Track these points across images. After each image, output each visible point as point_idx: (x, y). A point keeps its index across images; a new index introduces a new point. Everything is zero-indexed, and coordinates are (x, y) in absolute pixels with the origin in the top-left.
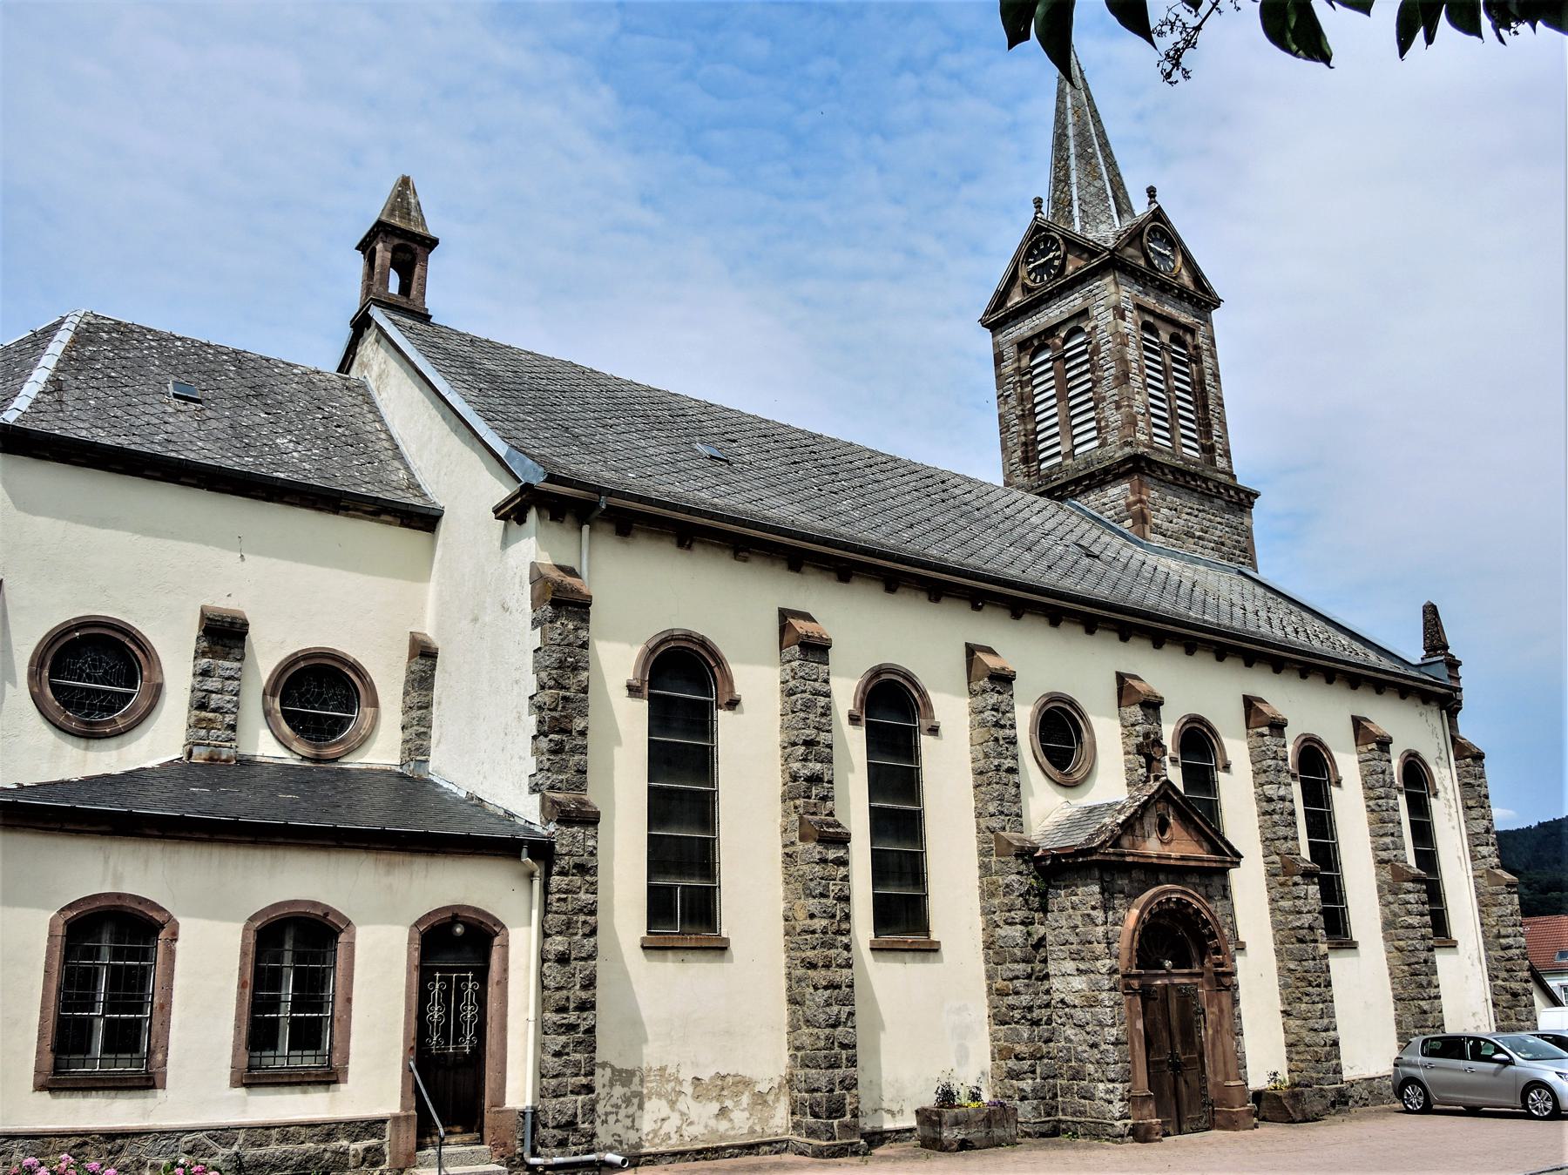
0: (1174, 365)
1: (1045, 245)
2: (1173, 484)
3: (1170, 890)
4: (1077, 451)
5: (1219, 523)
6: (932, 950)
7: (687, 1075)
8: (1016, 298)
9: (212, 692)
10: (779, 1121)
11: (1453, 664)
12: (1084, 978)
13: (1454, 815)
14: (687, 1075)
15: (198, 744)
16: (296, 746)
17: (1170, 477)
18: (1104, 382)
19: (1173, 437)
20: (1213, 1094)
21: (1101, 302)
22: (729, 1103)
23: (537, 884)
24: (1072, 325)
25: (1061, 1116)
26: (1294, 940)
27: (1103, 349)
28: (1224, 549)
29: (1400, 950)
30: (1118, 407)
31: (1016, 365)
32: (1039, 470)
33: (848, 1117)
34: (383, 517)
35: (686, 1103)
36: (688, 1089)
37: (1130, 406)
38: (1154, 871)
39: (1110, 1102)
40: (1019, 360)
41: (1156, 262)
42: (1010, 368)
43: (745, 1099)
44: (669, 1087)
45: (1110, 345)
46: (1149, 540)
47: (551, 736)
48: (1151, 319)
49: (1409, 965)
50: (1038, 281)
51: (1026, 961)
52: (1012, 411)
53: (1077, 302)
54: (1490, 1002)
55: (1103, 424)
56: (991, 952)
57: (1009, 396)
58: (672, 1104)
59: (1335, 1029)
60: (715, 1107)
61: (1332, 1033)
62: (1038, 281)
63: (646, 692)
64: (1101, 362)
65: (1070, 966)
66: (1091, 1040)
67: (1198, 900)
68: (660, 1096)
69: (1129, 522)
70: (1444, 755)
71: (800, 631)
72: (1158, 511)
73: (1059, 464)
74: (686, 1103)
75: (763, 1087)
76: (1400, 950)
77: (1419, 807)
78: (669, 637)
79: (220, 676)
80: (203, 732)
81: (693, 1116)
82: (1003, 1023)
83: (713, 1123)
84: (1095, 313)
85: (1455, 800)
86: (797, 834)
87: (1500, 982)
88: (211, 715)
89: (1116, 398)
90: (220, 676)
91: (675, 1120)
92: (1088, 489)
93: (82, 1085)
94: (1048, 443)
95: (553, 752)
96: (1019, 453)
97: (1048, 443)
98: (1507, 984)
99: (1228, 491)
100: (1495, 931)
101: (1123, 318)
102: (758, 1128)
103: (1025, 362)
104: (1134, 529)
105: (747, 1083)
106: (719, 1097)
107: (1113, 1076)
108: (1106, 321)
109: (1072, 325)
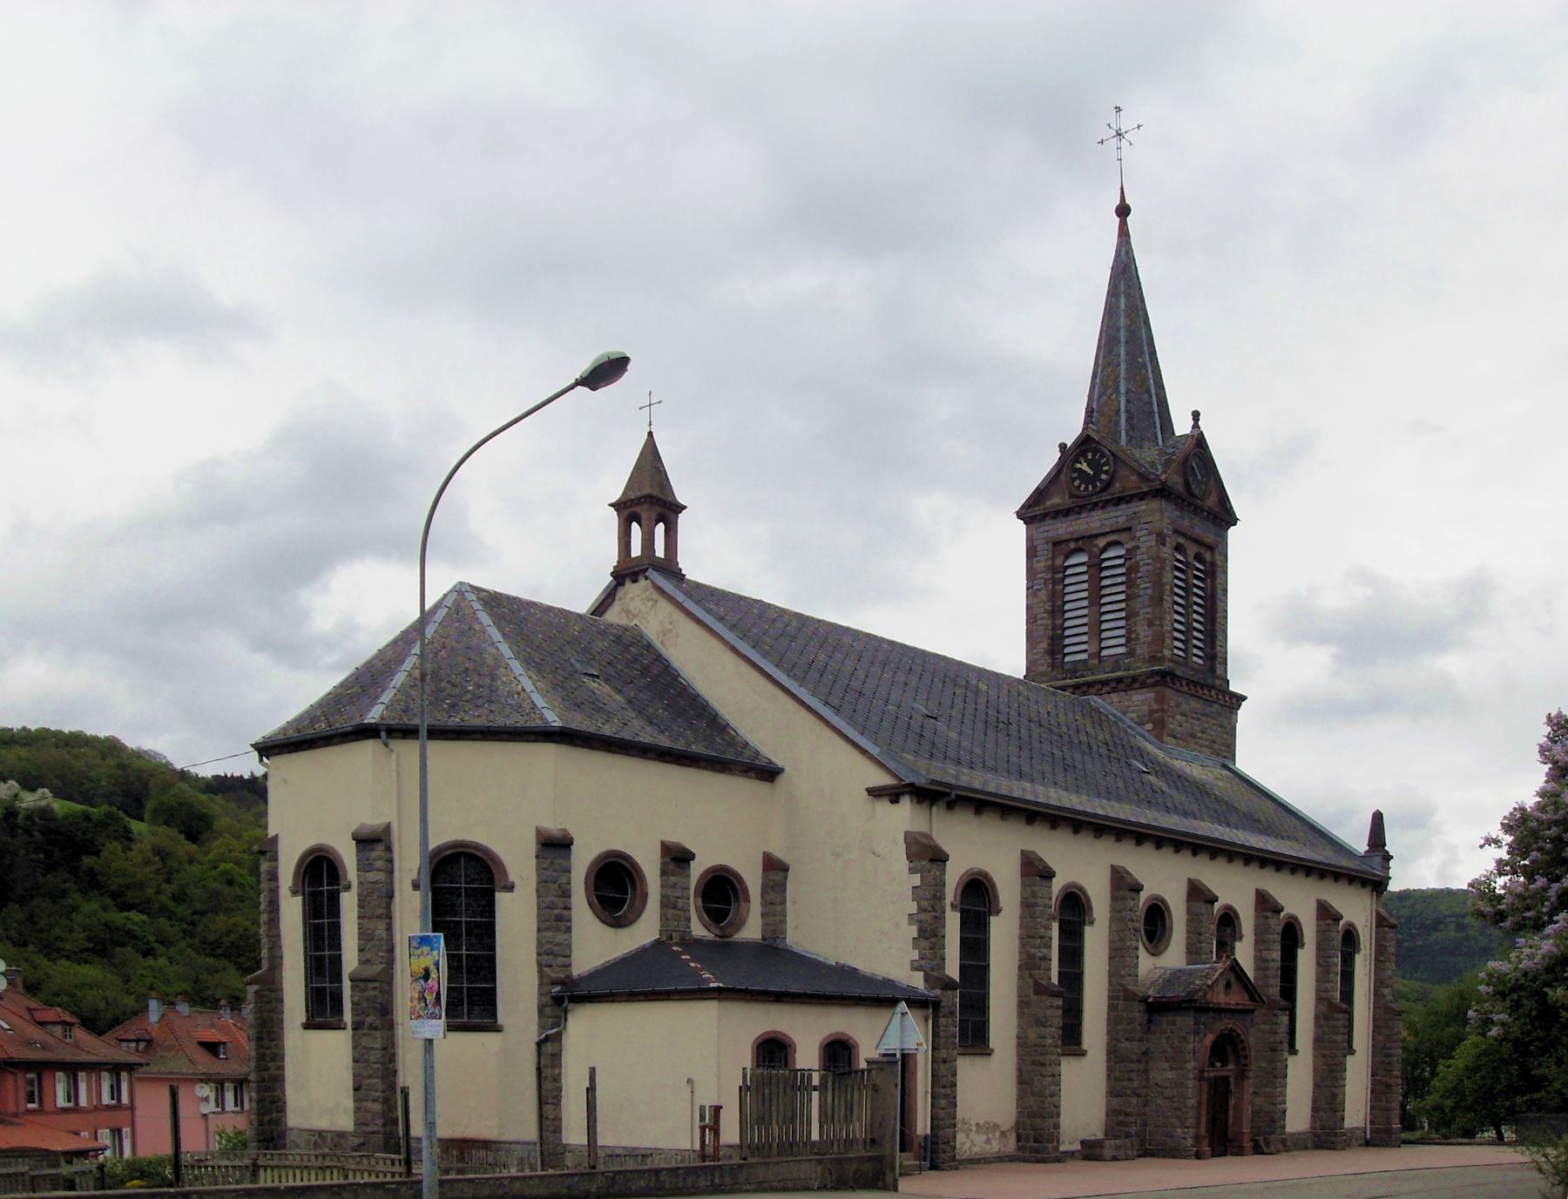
0: (1196, 582)
1: (1094, 456)
2: (1186, 694)
3: (1226, 1023)
4: (1104, 653)
5: (1214, 724)
6: (1083, 1054)
7: (973, 1123)
8: (1055, 501)
9: (679, 898)
10: (1011, 1145)
11: (1387, 858)
12: (1174, 1072)
13: (1368, 965)
14: (973, 1123)
15: (675, 931)
16: (712, 929)
17: (1185, 688)
18: (1140, 599)
19: (1187, 648)
20: (1230, 1134)
21: (1146, 526)
22: (990, 1136)
23: (930, 1022)
24: (1113, 538)
25: (1148, 1147)
26: (1268, 1049)
27: (1141, 569)
28: (1216, 746)
29: (1324, 1056)
30: (1150, 625)
31: (1050, 563)
32: (1063, 662)
33: (1055, 1143)
34: (750, 774)
35: (973, 1135)
36: (974, 1128)
37: (1161, 625)
38: (1220, 1011)
39: (1185, 1138)
40: (1053, 558)
41: (1193, 487)
42: (1043, 564)
43: (998, 1134)
44: (966, 1126)
45: (1150, 567)
46: (1165, 743)
47: (931, 939)
48: (1181, 540)
49: (1329, 1065)
50: (1082, 488)
51: (1139, 1061)
52: (1041, 605)
53: (1120, 520)
54: (1369, 1090)
55: (1133, 636)
56: (1112, 1056)
57: (1040, 590)
58: (967, 1135)
59: (1285, 1103)
60: (984, 1138)
61: (1283, 1105)
62: (1082, 488)
63: (959, 906)
64: (1138, 581)
65: (1166, 1065)
66: (1175, 1105)
67: (1240, 1029)
68: (962, 1131)
69: (1149, 726)
70: (1369, 924)
71: (1040, 867)
72: (1173, 717)
73: (1084, 661)
74: (973, 1135)
75: (1004, 1128)
76: (1324, 1056)
77: (1348, 962)
78: (986, 876)
79: (681, 888)
80: (676, 923)
81: (976, 1142)
82: (1117, 1096)
83: (983, 1145)
84: (1138, 534)
85: (1370, 956)
86: (1032, 990)
87: (1379, 1078)
88: (678, 912)
89: (1149, 616)
90: (681, 888)
91: (968, 1144)
92: (1114, 690)
93: (591, 1131)
94: (1075, 640)
95: (931, 949)
96: (1045, 645)
97: (1075, 640)
98: (1384, 1079)
99: (1224, 696)
100: (1381, 1045)
101: (1164, 544)
102: (1002, 1149)
103: (1059, 561)
104: (1154, 732)
105: (996, 1126)
106: (987, 1134)
107: (1189, 1125)
108: (1149, 544)
109: (1113, 538)
